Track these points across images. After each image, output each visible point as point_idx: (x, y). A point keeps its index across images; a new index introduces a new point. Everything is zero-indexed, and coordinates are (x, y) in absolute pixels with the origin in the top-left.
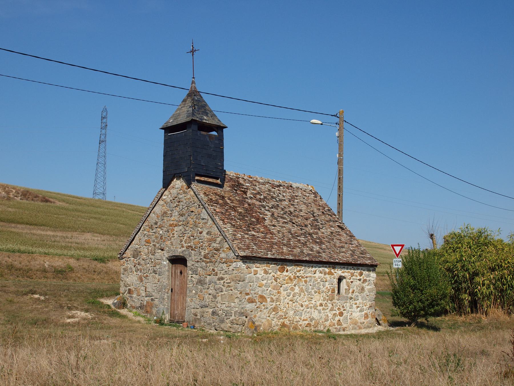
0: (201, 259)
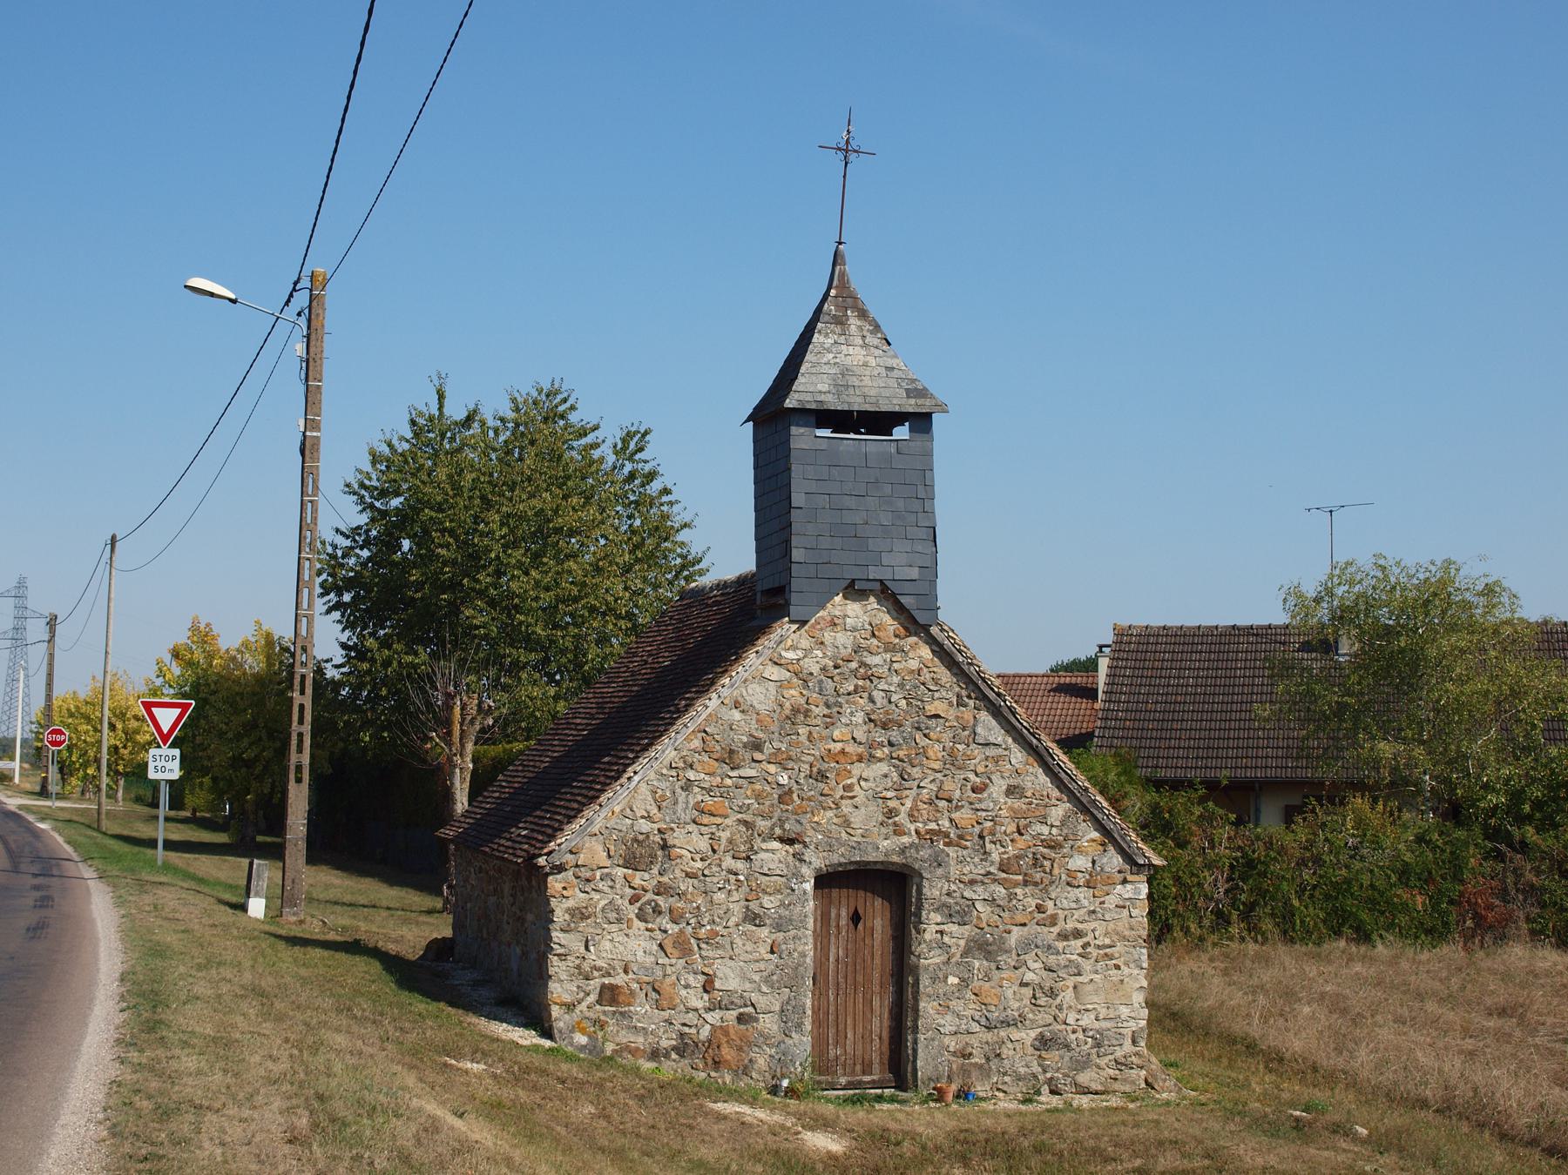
0: (989, 873)
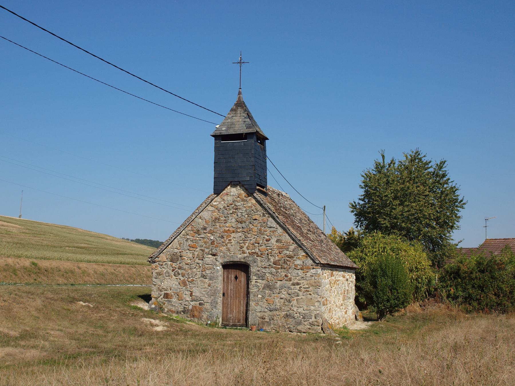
0: (270, 265)
